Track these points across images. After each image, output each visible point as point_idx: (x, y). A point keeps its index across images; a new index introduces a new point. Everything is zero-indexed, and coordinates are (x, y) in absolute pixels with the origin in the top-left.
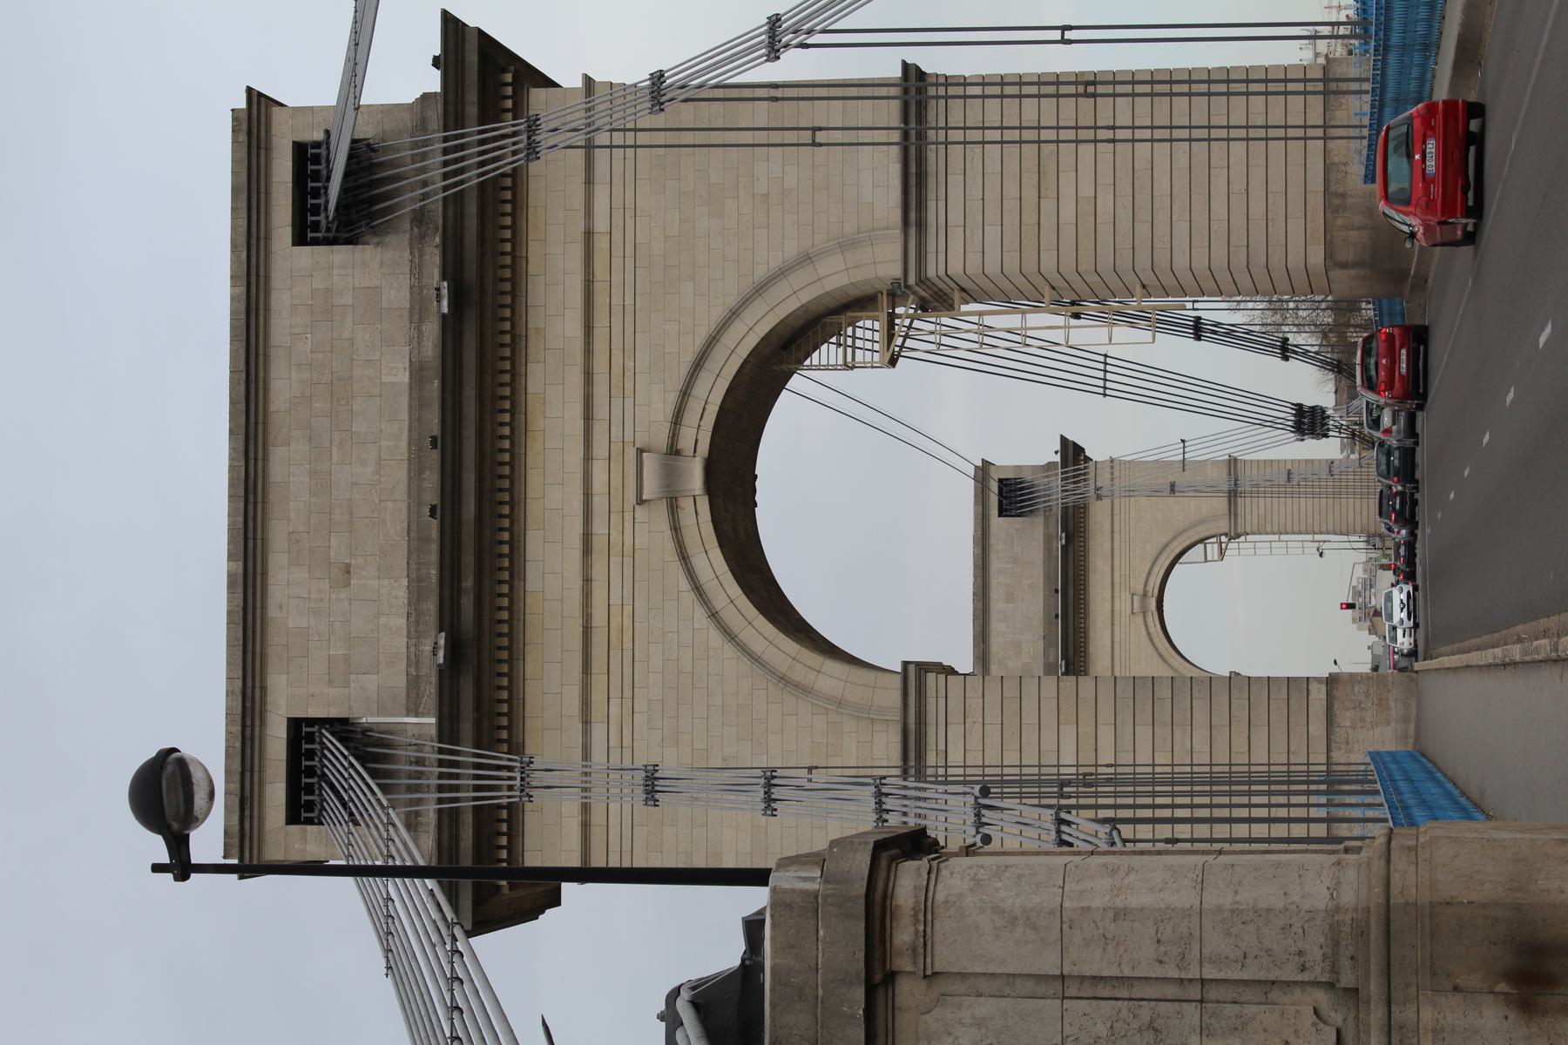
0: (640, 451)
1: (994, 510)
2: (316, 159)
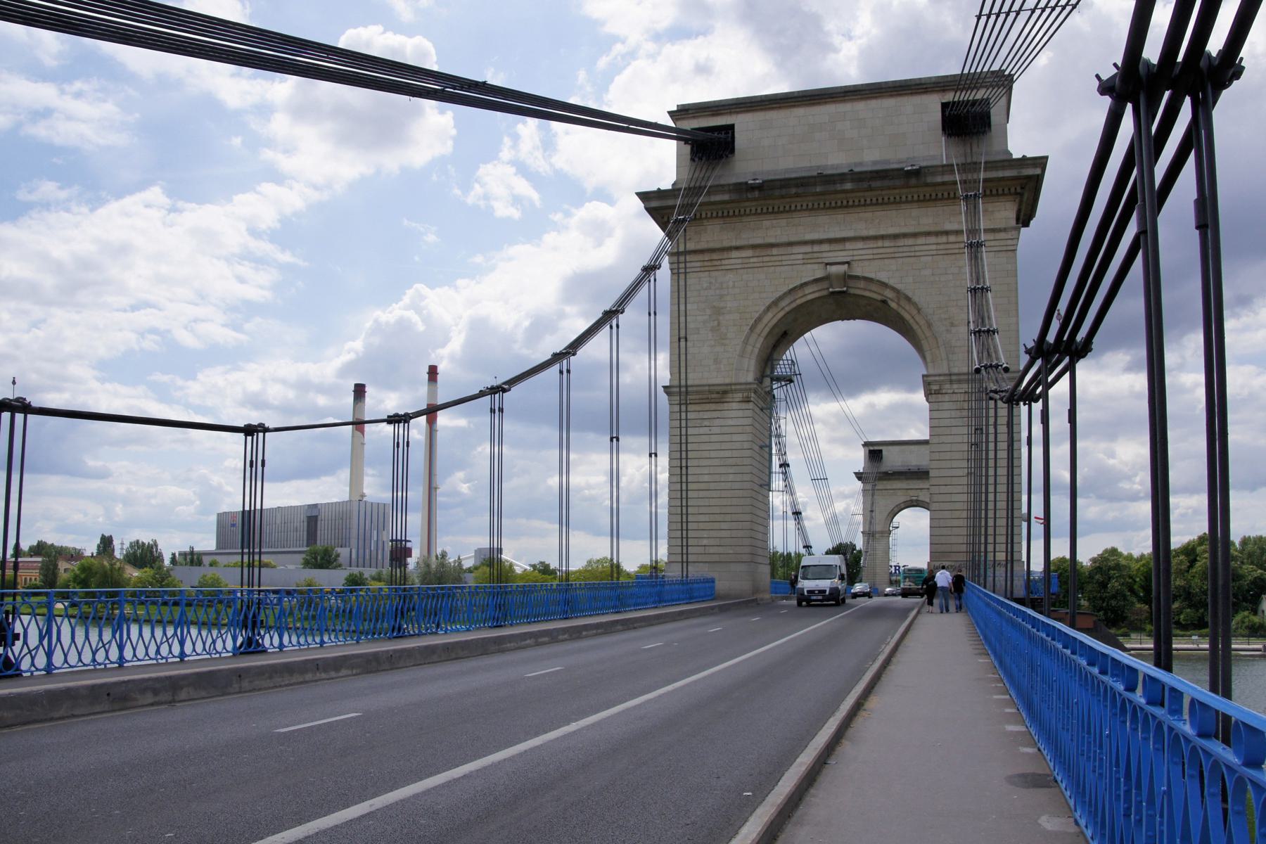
0: (848, 263)
1: (872, 448)
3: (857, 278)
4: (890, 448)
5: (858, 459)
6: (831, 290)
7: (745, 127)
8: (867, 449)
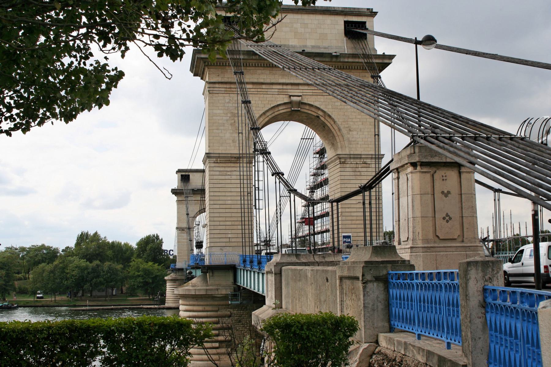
0: (301, 96)
1: (184, 174)
2: (363, 27)
3: (305, 104)
4: (195, 174)
5: (175, 182)
6: (293, 109)
7: (192, 176)
8: (180, 174)
